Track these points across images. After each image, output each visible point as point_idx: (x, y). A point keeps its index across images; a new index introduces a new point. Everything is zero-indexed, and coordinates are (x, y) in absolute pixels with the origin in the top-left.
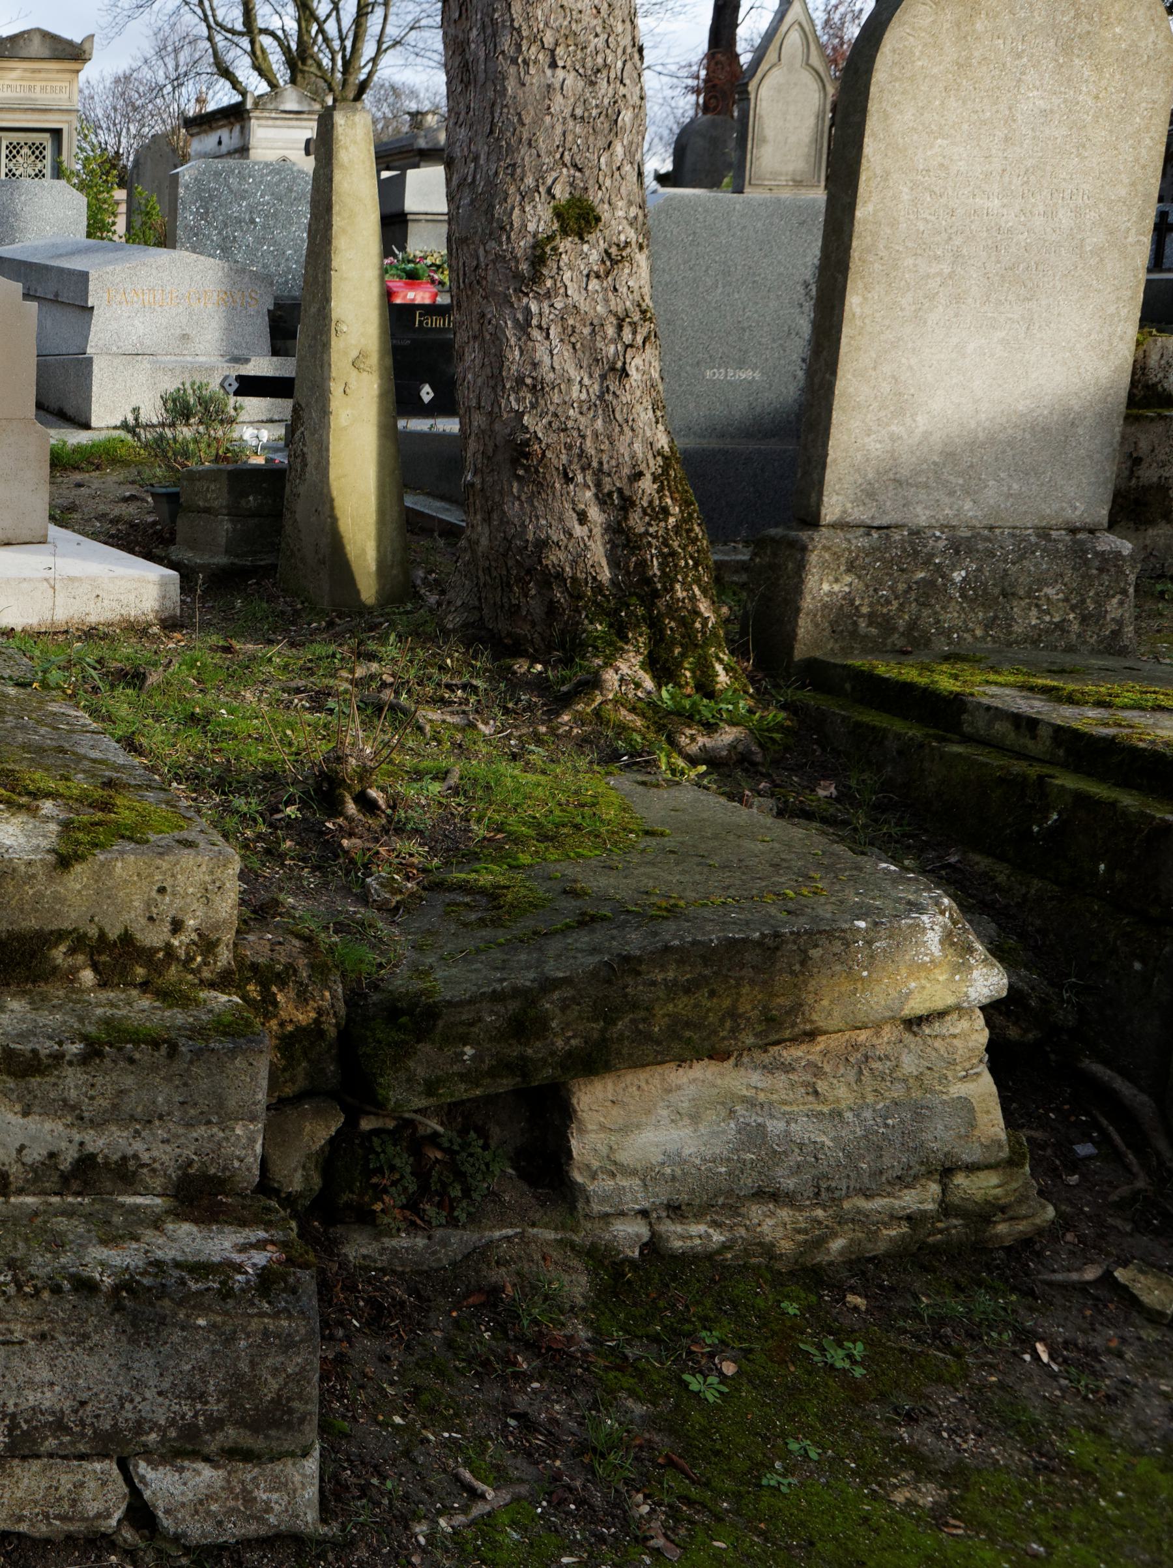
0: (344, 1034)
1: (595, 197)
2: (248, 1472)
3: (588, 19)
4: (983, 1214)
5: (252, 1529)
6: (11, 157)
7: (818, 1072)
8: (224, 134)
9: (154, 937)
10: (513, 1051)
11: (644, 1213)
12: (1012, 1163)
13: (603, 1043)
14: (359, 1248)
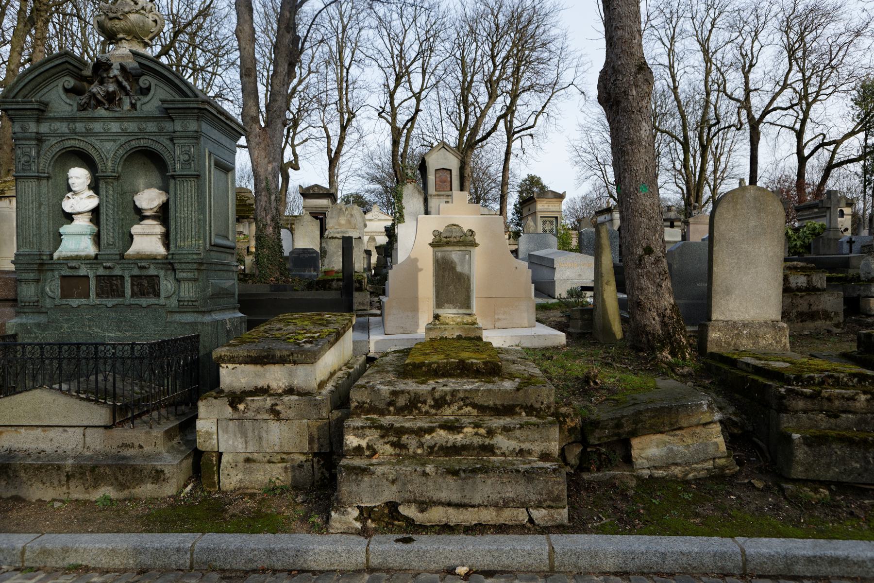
0: (582, 428)
1: (652, 246)
2: (552, 511)
3: (648, 207)
4: (722, 468)
5: (554, 523)
6: (544, 224)
7: (684, 436)
8: (606, 216)
9: (537, 406)
10: (616, 431)
11: (649, 468)
12: (728, 457)
13: (636, 429)
14: (586, 476)
